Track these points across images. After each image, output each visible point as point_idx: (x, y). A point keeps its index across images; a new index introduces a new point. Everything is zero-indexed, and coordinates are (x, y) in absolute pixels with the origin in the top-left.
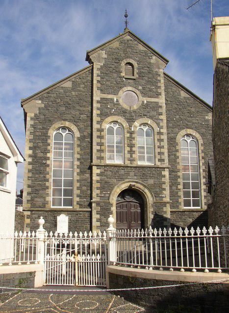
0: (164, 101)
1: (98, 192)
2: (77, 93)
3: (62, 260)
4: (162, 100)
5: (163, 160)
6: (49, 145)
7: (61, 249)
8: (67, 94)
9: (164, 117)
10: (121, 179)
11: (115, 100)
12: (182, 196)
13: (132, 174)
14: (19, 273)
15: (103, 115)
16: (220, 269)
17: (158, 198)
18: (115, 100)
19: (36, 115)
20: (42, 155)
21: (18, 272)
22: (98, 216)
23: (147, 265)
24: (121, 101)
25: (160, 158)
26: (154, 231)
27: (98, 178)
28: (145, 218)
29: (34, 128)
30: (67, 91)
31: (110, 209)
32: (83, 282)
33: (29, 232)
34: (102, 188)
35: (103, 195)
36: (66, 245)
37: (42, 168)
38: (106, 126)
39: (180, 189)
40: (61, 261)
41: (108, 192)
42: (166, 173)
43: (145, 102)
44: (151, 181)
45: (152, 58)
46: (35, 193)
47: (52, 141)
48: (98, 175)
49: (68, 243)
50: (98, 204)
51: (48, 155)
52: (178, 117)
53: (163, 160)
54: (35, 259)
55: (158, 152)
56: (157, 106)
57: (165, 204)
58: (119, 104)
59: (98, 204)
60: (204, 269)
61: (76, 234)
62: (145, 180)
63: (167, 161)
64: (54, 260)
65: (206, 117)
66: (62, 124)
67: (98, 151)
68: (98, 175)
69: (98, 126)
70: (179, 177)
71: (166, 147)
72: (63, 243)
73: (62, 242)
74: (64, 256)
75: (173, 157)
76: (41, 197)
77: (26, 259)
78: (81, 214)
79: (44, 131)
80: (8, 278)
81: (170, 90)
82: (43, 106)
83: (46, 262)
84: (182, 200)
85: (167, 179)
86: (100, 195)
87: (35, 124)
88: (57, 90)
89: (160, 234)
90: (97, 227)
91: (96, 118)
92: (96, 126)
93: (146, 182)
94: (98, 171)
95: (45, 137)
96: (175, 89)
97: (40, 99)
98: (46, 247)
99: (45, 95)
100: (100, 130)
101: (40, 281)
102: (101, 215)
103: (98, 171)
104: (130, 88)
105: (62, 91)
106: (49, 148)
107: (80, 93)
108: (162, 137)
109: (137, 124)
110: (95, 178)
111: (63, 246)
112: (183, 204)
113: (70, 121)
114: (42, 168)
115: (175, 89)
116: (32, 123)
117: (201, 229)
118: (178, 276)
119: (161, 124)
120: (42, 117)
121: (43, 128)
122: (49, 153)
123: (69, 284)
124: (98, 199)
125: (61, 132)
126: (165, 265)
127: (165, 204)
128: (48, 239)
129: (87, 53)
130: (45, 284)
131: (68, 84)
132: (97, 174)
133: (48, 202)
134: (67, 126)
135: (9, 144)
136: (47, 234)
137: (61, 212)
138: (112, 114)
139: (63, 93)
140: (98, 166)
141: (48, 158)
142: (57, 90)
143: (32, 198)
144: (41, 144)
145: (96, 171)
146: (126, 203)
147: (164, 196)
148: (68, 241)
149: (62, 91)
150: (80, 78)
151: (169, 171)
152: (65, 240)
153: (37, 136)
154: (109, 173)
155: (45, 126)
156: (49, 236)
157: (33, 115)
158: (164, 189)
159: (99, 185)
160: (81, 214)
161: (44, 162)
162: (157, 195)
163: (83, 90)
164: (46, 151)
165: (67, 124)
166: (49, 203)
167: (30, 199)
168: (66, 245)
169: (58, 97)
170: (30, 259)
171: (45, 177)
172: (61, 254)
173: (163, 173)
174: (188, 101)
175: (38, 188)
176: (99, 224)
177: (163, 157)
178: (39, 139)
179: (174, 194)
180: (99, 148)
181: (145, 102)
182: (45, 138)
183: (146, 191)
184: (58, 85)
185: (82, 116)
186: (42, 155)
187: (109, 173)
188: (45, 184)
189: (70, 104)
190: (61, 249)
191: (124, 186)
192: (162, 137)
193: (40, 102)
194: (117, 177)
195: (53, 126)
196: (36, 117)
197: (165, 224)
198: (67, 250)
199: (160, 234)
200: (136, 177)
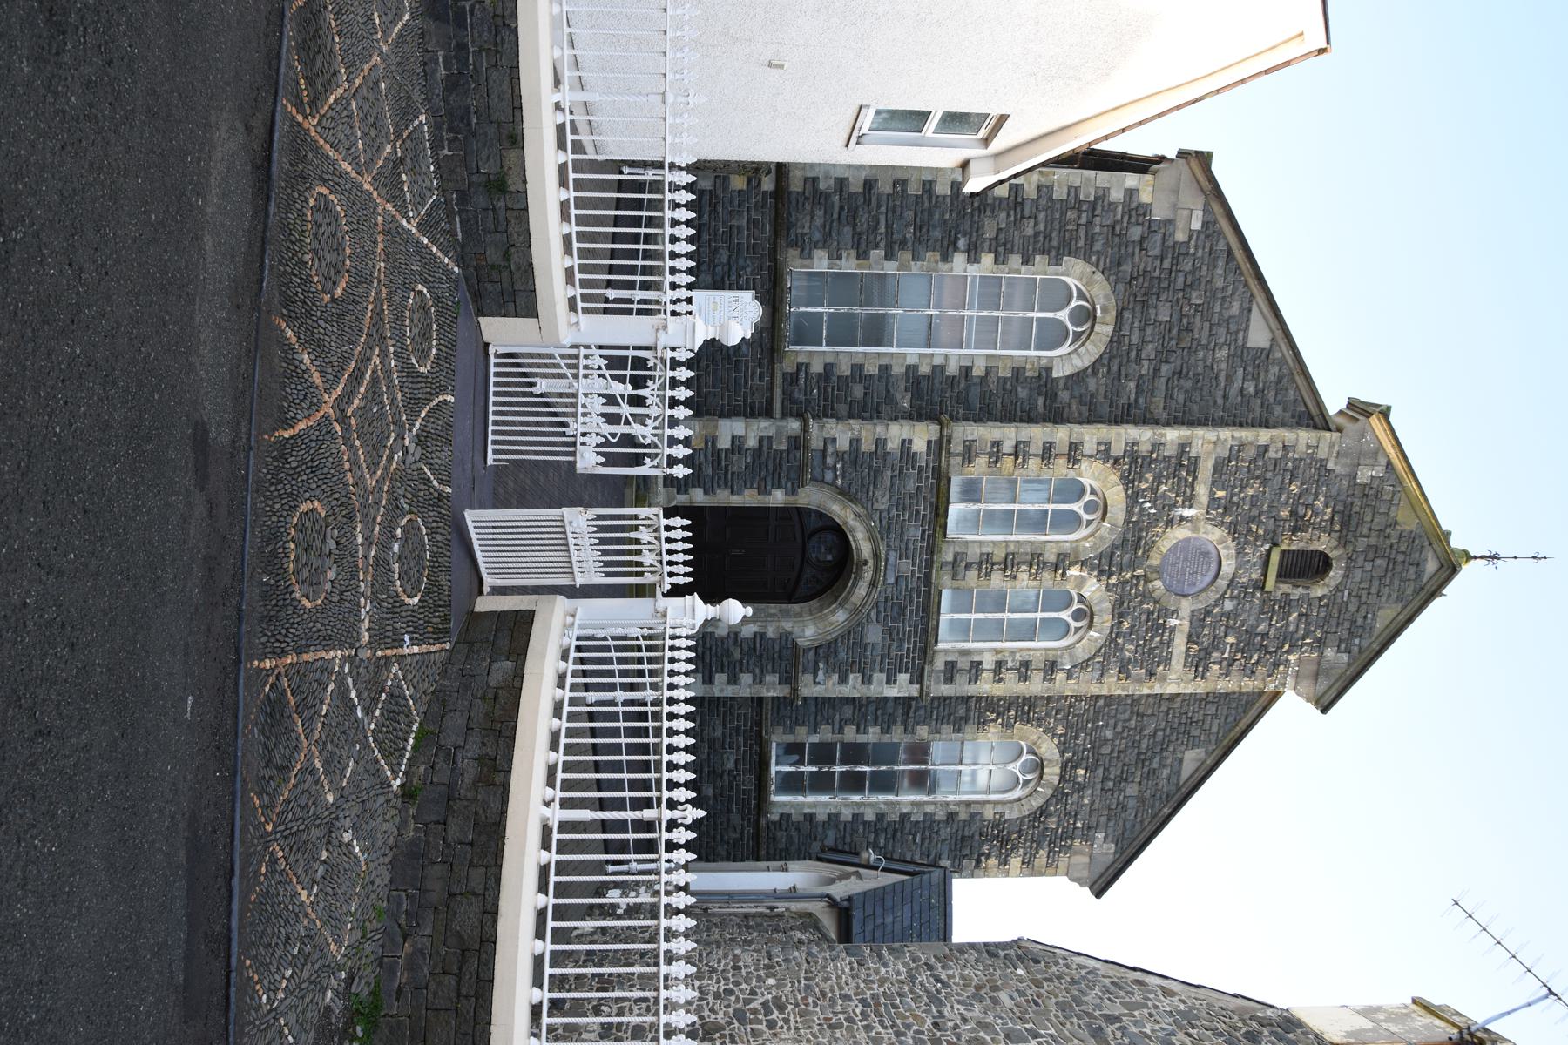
0: (1171, 689)
1: (843, 444)
2: (1223, 366)
3: (586, 376)
4: (1176, 681)
5: (950, 679)
6: (1026, 262)
7: (629, 373)
8: (1222, 331)
9: (1112, 686)
10: (885, 529)
11: (1187, 512)
12: (815, 739)
13: (906, 566)
14: (531, 265)
15: (1132, 465)
16: (550, 901)
17: (811, 655)
18: (1187, 512)
19: (1145, 209)
20: (989, 234)
21: (535, 261)
22: (752, 443)
23: (559, 794)
24: (1179, 533)
25: (960, 665)
26: (687, 828)
27: (893, 445)
28: (739, 864)
29: (1093, 205)
30: (1233, 328)
31: (779, 487)
32: (506, 365)
33: (690, 694)
34: (854, 456)
35: (829, 461)
36: (640, 392)
37: (937, 234)
38: (1091, 474)
39: (841, 730)
40: (582, 372)
41: (839, 482)
42: (903, 687)
43: (1173, 622)
44: (874, 634)
45: (1339, 651)
46: (842, 208)
47: (1041, 270)
48: (906, 444)
49: (649, 402)
50: (799, 443)
51: (987, 259)
52: (1109, 734)
53: (950, 679)
54: (586, 311)
55: (980, 663)
56: (1153, 662)
57: (790, 679)
58: (1170, 523)
59: (799, 443)
60: (540, 987)
61: (683, 393)
62: (878, 613)
63: (947, 690)
64: (586, 367)
65: (1101, 836)
66: (1104, 310)
67: (997, 444)
68: (906, 444)
69: (1089, 447)
70: (886, 730)
71: (998, 690)
72: (650, 383)
73: (651, 378)
74: (598, 385)
75: (961, 712)
76: (827, 234)
77: (584, 284)
78: (761, 377)
79: (1081, 244)
80: (514, 227)
81: (1211, 709)
82: (1181, 237)
83: (574, 351)
84: (803, 735)
85: (880, 688)
86: (830, 450)
87: (1110, 204)
88: (1241, 289)
89: (676, 814)
90: (714, 440)
91: (1122, 436)
92: (1090, 436)
93: (873, 615)
94: (919, 446)
95: (1057, 246)
96: (1214, 729)
97: (1205, 224)
98: (630, 353)
99: (1221, 246)
100: (1074, 453)
101: (501, 333)
102: (758, 452)
103: (919, 446)
104: (1228, 567)
105: (1235, 308)
106: (1015, 260)
107: (1222, 378)
108: (1037, 677)
109: (1093, 588)
110: (895, 433)
111: (639, 383)
112: (790, 738)
113: (1116, 340)
114: (937, 234)
115: (1214, 729)
116: (1117, 195)
117: (689, 256)
118: (543, 656)
119: (1085, 676)
120: (1136, 233)
121: (1091, 239)
122: (996, 261)
123: (495, 442)
124: (816, 443)
125: (1074, 303)
126: (572, 676)
127: (790, 679)
128: (663, 361)
129: (1385, 413)
130: (491, 351)
131: (1258, 336)
132: (910, 441)
133: (810, 256)
134: (1097, 328)
135: (1044, 142)
136: (682, 356)
137: (772, 299)
138: (1133, 499)
139: (1226, 314)
140: (939, 447)
141: (973, 258)
142: (1241, 289)
143: (826, 195)
144: (1029, 231)
145: (921, 436)
146: (799, 540)
147: (821, 676)
148: (657, 400)
149: (1235, 308)
150: (1279, 380)
151: (910, 698)
152: (662, 387)
153: (1063, 214)
154: (912, 485)
155: (1098, 246)
156: (675, 364)
157: (1145, 197)
158: (843, 680)
159: (867, 446)
160: (761, 377)
161: (962, 243)
162: (826, 652)
163: (1234, 391)
164: (1001, 250)
165: (1105, 330)
166: (807, 262)
167: (822, 186)
168: (640, 392)
169: (1211, 294)
170: (585, 298)
171: (903, 244)
172: (607, 373)
173: (903, 678)
174: (1166, 772)
175: (863, 218)
176: (724, 443)
177: (961, 679)
178: (1049, 222)
179: (825, 708)
180: (1008, 447)
181: (1173, 622)
182: (1055, 243)
183: (840, 616)
184: (1260, 299)
185: (1132, 386)
186: (989, 234)
187: (912, 485)
188: (877, 247)
189: (1179, 340)
190: (629, 373)
191: (862, 544)
192: (1037, 677)
193: (1196, 225)
194: (894, 512)
195: (1099, 276)
196: (1136, 211)
197: (717, 676)
198: (622, 396)
199: (676, 814)
200: (891, 580)
